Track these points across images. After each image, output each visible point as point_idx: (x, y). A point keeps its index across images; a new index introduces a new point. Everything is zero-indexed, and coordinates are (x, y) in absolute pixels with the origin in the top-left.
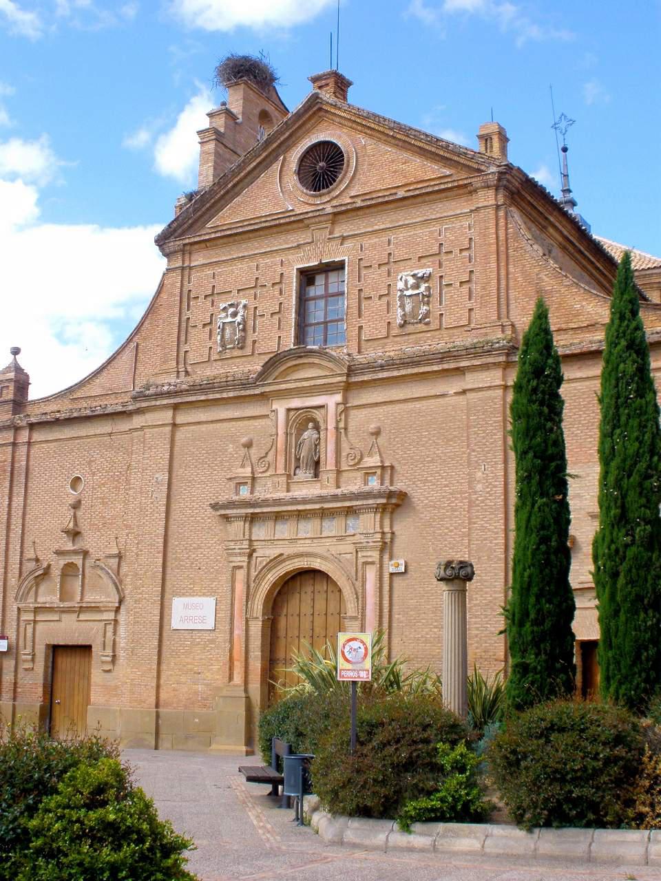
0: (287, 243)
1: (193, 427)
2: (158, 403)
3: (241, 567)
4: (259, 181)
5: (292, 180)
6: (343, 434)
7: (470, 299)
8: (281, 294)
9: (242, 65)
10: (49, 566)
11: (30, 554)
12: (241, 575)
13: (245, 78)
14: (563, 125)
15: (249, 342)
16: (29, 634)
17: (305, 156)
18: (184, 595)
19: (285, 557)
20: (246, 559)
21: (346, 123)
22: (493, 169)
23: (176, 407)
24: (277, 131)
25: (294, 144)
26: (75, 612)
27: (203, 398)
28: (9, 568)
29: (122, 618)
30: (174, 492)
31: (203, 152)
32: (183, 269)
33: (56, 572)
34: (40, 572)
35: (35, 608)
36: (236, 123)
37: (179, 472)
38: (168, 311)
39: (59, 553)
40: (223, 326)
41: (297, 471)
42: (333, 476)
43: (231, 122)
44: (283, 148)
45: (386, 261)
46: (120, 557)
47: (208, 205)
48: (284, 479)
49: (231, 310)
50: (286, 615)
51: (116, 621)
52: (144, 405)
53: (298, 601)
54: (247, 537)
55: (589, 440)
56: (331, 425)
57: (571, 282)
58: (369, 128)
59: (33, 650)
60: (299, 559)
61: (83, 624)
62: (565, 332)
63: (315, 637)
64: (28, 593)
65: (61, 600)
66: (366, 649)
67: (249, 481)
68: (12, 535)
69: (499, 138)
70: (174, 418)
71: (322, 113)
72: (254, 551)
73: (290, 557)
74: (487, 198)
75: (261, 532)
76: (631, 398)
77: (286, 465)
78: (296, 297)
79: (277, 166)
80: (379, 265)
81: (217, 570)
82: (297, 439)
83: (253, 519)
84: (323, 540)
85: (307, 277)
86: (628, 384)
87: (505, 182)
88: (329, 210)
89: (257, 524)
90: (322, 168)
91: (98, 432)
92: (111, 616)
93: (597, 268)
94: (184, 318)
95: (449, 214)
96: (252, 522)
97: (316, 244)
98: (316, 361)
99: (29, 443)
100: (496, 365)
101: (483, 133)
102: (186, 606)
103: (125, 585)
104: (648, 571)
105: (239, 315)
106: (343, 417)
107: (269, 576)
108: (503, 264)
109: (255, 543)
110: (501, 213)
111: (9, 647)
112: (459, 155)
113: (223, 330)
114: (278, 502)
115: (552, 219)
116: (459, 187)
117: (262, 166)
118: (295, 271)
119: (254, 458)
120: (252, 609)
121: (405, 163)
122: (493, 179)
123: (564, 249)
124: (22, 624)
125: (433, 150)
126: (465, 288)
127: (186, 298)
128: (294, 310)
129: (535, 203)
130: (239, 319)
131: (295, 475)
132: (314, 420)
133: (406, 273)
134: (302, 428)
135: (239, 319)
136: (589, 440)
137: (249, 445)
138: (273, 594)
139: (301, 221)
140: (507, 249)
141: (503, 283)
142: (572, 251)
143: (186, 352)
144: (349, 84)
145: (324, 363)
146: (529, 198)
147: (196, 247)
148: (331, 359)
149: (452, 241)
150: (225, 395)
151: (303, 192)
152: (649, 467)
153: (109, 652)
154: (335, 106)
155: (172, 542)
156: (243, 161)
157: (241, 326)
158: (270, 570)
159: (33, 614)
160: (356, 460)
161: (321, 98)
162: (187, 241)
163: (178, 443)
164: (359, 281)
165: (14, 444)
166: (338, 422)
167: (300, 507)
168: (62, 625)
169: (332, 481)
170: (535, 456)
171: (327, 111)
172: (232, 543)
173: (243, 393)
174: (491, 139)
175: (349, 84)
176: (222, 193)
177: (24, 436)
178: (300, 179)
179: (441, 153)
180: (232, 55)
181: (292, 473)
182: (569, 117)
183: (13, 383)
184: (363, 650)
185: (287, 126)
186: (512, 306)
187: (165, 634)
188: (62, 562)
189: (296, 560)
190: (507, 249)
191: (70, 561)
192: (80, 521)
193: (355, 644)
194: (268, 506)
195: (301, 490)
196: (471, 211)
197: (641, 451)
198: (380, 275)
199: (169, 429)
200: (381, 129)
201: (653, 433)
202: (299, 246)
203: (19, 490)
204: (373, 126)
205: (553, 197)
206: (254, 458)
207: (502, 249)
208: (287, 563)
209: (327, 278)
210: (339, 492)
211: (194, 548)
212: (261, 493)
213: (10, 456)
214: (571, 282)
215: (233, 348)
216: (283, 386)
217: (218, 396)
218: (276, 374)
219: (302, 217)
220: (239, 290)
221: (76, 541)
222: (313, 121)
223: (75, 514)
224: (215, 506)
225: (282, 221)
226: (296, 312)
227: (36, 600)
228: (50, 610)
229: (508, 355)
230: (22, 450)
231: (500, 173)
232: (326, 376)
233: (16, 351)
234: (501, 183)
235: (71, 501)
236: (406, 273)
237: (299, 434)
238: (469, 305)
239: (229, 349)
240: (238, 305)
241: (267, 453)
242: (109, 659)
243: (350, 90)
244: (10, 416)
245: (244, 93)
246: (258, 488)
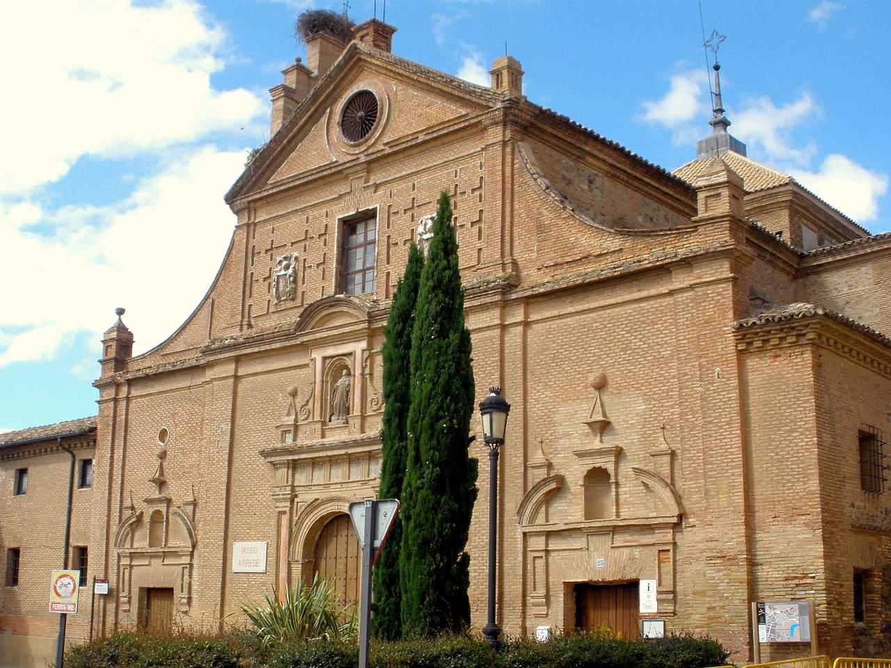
0: (332, 195)
1: (252, 378)
2: (222, 356)
3: (285, 512)
4: (311, 134)
5: (336, 131)
6: (368, 381)
7: (479, 239)
8: (325, 245)
9: (315, 20)
10: (142, 513)
11: (127, 503)
12: (285, 520)
13: (321, 32)
14: (715, 41)
15: (299, 294)
16: (127, 575)
17: (347, 108)
18: (242, 540)
19: (319, 501)
20: (288, 504)
21: (381, 70)
22: (499, 105)
23: (237, 360)
24: (322, 85)
25: (340, 96)
26: (160, 557)
27: (256, 350)
28: (112, 516)
29: (195, 562)
30: (236, 442)
31: (275, 110)
32: (248, 225)
33: (147, 519)
34: (134, 519)
35: (131, 553)
36: (310, 77)
37: (240, 421)
38: (240, 263)
39: (149, 501)
40: (278, 278)
41: (333, 418)
42: (358, 421)
43: (305, 78)
44: (330, 101)
45: (411, 206)
46: (195, 504)
47: (268, 162)
48: (319, 426)
49: (285, 263)
50: (326, 558)
51: (191, 565)
52: (212, 358)
53: (335, 545)
54: (290, 483)
55: (578, 376)
56: (358, 372)
57: (568, 214)
58: (399, 74)
59: (130, 593)
60: (331, 504)
61: (167, 567)
62: (561, 266)
63: (348, 580)
64: (125, 541)
65: (151, 545)
66: (75, 585)
67: (292, 429)
68: (114, 485)
69: (508, 72)
70: (236, 370)
71: (360, 64)
72: (296, 496)
73: (325, 502)
74: (495, 135)
75: (301, 478)
76: (432, 340)
77: (321, 412)
78: (338, 247)
79: (324, 119)
80: (405, 210)
81: (268, 516)
82: (332, 387)
83: (295, 466)
84: (350, 485)
85: (349, 226)
86: (431, 325)
87: (511, 117)
88: (363, 159)
89: (299, 470)
90: (360, 118)
91: (180, 385)
92: (186, 560)
93: (665, 194)
94: (249, 273)
95: (465, 154)
96: (294, 469)
97: (354, 194)
98: (345, 309)
99: (128, 399)
100: (494, 304)
101: (495, 68)
102: (244, 551)
103: (198, 531)
104: (436, 513)
105: (291, 267)
106: (368, 363)
107: (308, 520)
108: (508, 201)
109: (297, 489)
110: (508, 149)
111: (110, 590)
112: (470, 93)
113: (278, 282)
114: (311, 449)
115: (587, 148)
116: (471, 126)
117: (312, 121)
118: (337, 221)
119: (298, 406)
120: (294, 553)
121: (428, 106)
122: (499, 115)
123: (613, 176)
124: (122, 568)
125: (450, 90)
126: (475, 229)
127: (251, 254)
128: (335, 260)
129: (560, 135)
130: (290, 271)
131: (330, 421)
132: (346, 367)
133: (426, 217)
134: (336, 378)
135: (290, 271)
136: (578, 376)
137: (294, 394)
138: (314, 538)
139: (340, 172)
140: (513, 185)
141: (508, 219)
142: (626, 178)
143: (250, 306)
144: (392, 31)
145: (351, 311)
146: (550, 130)
147: (259, 203)
148: (356, 307)
149: (466, 181)
150: (273, 346)
151: (344, 142)
152: (440, 408)
153: (185, 594)
154: (370, 54)
155: (234, 489)
156: (295, 117)
157: (291, 279)
158: (308, 515)
159: (129, 559)
160: (379, 405)
161: (359, 49)
162: (250, 199)
163: (240, 395)
164: (388, 228)
165: (116, 400)
166: (363, 368)
167: (330, 453)
168: (151, 569)
169: (358, 426)
170: (396, 400)
171: (365, 61)
172: (278, 489)
173: (287, 344)
174: (501, 73)
175: (392, 31)
176: (279, 149)
177: (125, 389)
178: (343, 130)
179: (456, 93)
180: (307, 11)
181: (328, 420)
182: (720, 33)
183: (115, 342)
184: (71, 586)
185: (331, 78)
186: (516, 244)
187: (228, 577)
188: (151, 511)
189: (329, 505)
190: (513, 185)
191: (157, 509)
192: (166, 471)
193: (66, 580)
194: (304, 453)
195: (333, 436)
196: (483, 149)
197: (433, 393)
198: (405, 220)
199: (232, 380)
200: (407, 74)
201: (450, 374)
202: (340, 197)
203: (120, 442)
204: (400, 71)
205: (580, 126)
206: (298, 406)
207: (508, 185)
208: (322, 507)
209: (366, 227)
210: (365, 436)
211: (251, 495)
212: (303, 441)
213: (112, 411)
214: (568, 214)
215: (286, 300)
216: (318, 336)
217: (268, 347)
218: (313, 323)
219: (341, 168)
220: (292, 244)
221: (163, 490)
222: (354, 72)
223: (161, 464)
224: (264, 454)
225: (325, 173)
226: (337, 261)
227: (132, 546)
228: (142, 555)
229: (503, 294)
230: (123, 404)
231: (505, 108)
232: (350, 324)
233: (121, 312)
234: (508, 119)
235: (158, 452)
236: (426, 217)
237: (335, 379)
238: (478, 246)
239: (284, 300)
240: (291, 258)
241: (308, 401)
242: (185, 601)
243: (395, 39)
244: (112, 373)
245: (321, 46)
246: (300, 435)
